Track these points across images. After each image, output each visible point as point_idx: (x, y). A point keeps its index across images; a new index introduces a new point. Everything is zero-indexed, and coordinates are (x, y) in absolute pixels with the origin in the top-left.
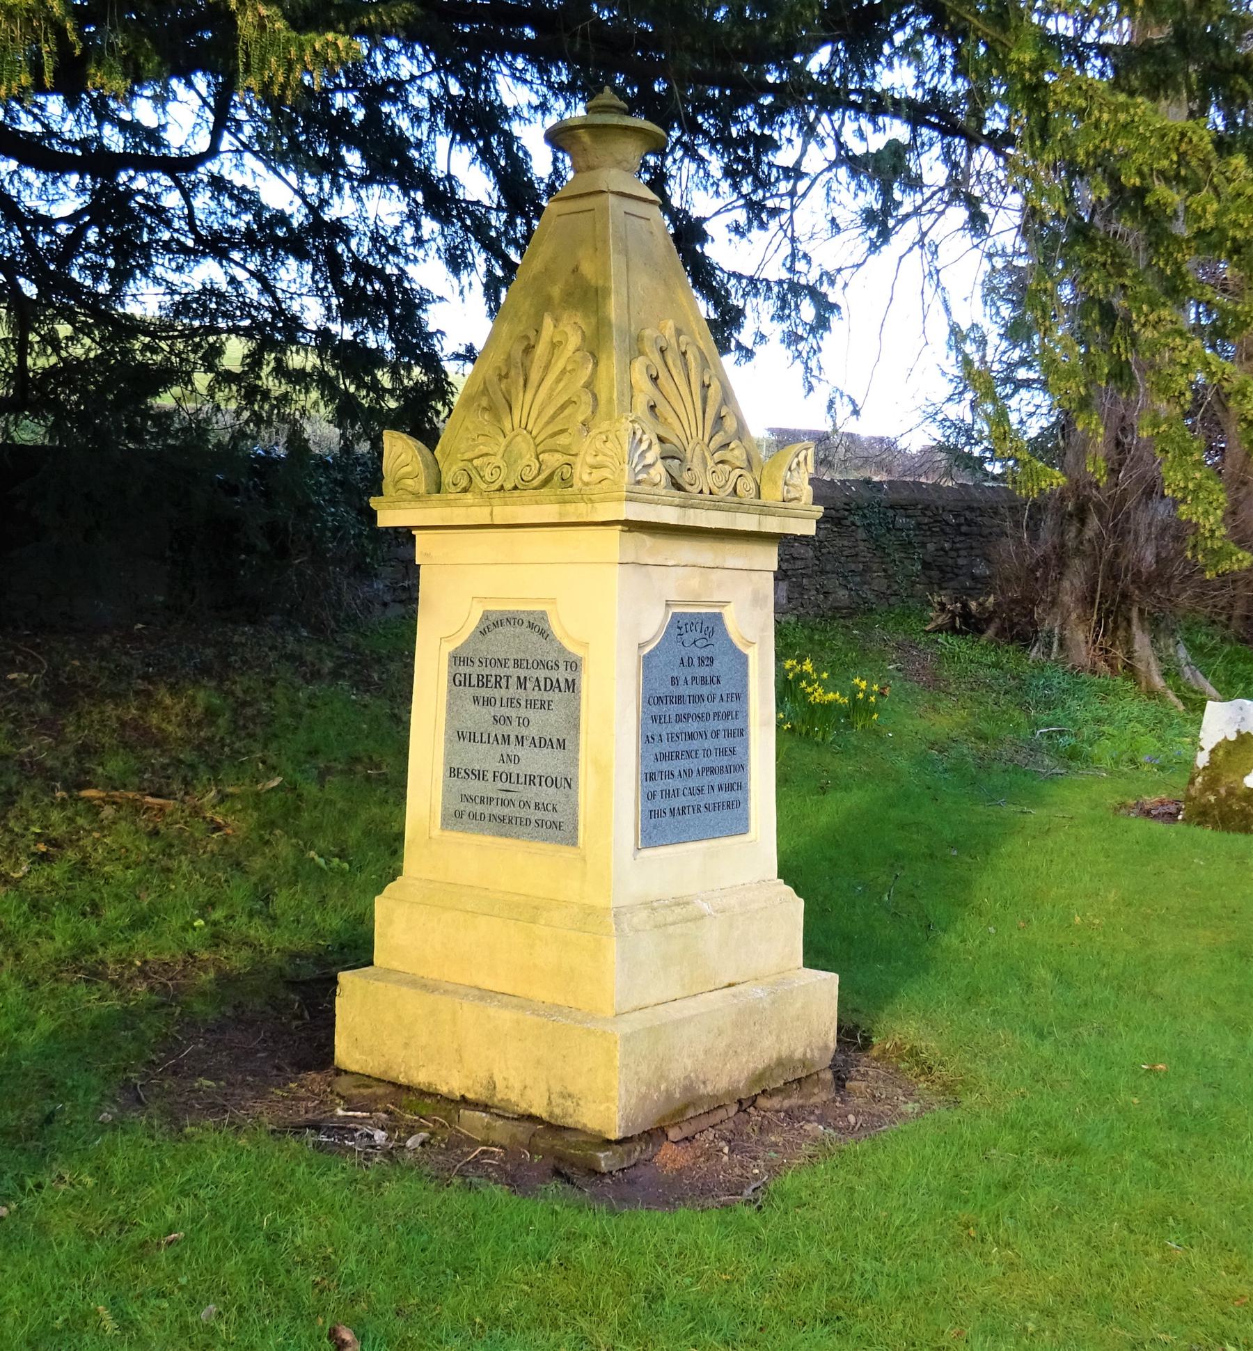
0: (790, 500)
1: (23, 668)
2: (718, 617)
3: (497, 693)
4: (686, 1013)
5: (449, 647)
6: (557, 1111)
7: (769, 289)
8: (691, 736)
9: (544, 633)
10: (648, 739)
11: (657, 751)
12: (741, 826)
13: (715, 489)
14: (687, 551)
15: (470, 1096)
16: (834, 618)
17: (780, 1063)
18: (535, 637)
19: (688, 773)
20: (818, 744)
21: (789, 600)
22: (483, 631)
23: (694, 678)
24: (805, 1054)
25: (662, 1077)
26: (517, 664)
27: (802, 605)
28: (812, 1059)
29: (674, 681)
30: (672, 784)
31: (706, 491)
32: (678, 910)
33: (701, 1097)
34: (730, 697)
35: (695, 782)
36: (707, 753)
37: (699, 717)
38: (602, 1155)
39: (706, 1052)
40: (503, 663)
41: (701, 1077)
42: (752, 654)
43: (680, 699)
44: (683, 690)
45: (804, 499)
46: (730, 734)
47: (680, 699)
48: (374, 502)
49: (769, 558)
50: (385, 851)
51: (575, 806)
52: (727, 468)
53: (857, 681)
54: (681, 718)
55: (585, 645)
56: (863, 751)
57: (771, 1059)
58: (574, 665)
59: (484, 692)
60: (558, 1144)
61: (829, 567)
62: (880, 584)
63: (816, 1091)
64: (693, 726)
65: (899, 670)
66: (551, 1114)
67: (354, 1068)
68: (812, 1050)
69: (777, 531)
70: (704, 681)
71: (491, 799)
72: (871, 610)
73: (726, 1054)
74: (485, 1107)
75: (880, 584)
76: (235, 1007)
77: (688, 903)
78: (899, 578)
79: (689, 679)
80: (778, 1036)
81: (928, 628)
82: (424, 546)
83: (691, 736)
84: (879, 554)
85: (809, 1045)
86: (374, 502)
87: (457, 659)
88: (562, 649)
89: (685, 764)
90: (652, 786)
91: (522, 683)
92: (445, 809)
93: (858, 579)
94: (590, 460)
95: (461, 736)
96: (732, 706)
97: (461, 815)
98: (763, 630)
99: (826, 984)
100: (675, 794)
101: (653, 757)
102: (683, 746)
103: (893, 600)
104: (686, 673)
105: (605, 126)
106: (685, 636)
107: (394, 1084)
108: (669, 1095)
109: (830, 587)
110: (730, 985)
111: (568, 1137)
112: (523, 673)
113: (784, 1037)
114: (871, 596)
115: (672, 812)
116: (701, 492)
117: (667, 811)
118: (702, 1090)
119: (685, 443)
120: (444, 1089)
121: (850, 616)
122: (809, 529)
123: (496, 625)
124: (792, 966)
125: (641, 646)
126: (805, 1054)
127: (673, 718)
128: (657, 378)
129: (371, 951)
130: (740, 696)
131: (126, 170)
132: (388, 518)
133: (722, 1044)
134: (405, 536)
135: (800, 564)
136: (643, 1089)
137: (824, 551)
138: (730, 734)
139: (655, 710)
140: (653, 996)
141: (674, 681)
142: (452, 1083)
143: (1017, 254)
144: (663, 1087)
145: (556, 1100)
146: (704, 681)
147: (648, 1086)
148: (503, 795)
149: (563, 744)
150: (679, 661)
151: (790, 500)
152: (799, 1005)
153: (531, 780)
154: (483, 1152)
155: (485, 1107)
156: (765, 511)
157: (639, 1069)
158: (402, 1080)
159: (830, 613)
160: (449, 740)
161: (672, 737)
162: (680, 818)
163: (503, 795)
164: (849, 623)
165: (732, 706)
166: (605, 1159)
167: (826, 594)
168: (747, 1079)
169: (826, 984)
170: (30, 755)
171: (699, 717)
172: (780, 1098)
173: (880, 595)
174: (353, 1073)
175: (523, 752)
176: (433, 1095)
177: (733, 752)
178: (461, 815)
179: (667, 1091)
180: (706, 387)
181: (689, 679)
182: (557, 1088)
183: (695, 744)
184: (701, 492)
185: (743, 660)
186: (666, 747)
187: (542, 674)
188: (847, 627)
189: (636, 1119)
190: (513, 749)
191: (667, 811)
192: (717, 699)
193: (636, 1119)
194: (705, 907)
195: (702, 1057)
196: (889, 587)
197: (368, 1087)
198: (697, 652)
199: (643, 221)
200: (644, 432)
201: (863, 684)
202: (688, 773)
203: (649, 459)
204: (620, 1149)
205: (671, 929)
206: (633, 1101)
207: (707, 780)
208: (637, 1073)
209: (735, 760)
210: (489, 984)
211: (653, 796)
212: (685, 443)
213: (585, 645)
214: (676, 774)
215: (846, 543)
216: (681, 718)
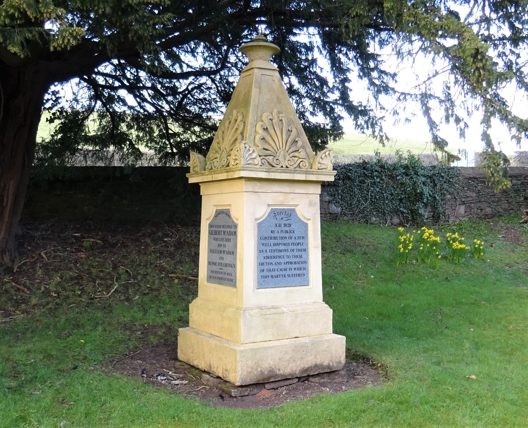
0: (322, 169)
1: (171, 237)
2: (294, 210)
3: (219, 237)
4: (271, 345)
5: (208, 222)
6: (225, 375)
7: (417, 96)
8: (281, 251)
9: (229, 216)
10: (260, 251)
11: (265, 256)
12: (306, 283)
13: (288, 166)
14: (276, 187)
15: (206, 370)
16: (485, 219)
17: (316, 366)
18: (227, 217)
19: (280, 264)
20: (456, 264)
21: (465, 212)
22: (216, 216)
23: (282, 231)
24: (329, 364)
25: (258, 366)
26: (223, 226)
27: (471, 214)
28: (333, 366)
29: (272, 232)
30: (272, 267)
31: (284, 166)
32: (273, 310)
33: (276, 375)
34: (299, 238)
35: (283, 266)
36: (288, 257)
37: (285, 244)
38: (232, 390)
39: (279, 359)
40: (220, 226)
41: (278, 368)
42: (310, 223)
43: (275, 238)
44: (276, 235)
45: (328, 169)
46: (300, 250)
47: (275, 238)
48: (187, 175)
49: (318, 190)
50: (190, 288)
51: (236, 274)
52: (296, 159)
53: (476, 240)
54: (275, 245)
55: (238, 219)
56: (474, 266)
57: (312, 364)
58: (236, 226)
59: (216, 236)
60: (223, 386)
61: (482, 200)
62: (506, 206)
63: (336, 377)
64: (282, 247)
65: (503, 237)
66: (223, 376)
67: (182, 360)
68: (333, 363)
69: (273, 178)
70: (287, 232)
71: (217, 272)
72: (501, 216)
73: (289, 361)
74: (209, 373)
75: (506, 206)
76: (165, 340)
77: (278, 308)
78: (514, 203)
79: (280, 231)
80: (315, 356)
81: (521, 222)
82: (203, 191)
83: (281, 251)
84: (504, 194)
85: (332, 360)
86: (187, 175)
87: (210, 226)
88: (233, 221)
89: (278, 260)
90: (262, 267)
91: (224, 232)
92: (208, 275)
93: (495, 204)
94: (234, 157)
95: (211, 251)
96: (301, 241)
97: (210, 278)
98: (314, 214)
99: (342, 339)
100: (274, 270)
101: (263, 258)
102: (276, 254)
103: (511, 212)
104: (277, 229)
105: (253, 46)
106: (277, 216)
107: (190, 365)
108: (262, 373)
109: (483, 207)
110: (296, 337)
111: (228, 384)
112: (224, 229)
113: (318, 357)
114: (500, 210)
115: (272, 277)
116: (282, 167)
117: (270, 276)
118: (278, 372)
119: (277, 150)
120: (200, 367)
121: (492, 217)
122: (332, 179)
123: (226, 214)
124: (327, 332)
125: (256, 220)
126: (329, 364)
127: (272, 245)
128: (267, 128)
129: (188, 323)
130: (305, 237)
131: (166, 79)
132: (192, 180)
133: (287, 357)
134: (197, 187)
135: (470, 199)
136: (250, 370)
137: (481, 194)
138: (300, 250)
139: (264, 241)
140: (260, 338)
141: (272, 232)
142: (202, 366)
143: (128, 70)
144: (259, 370)
145: (225, 372)
146: (287, 232)
147: (252, 368)
148: (220, 270)
149: (233, 253)
150: (275, 225)
151: (322, 169)
152: (325, 346)
153: (226, 265)
154: (204, 388)
155: (209, 373)
156: (307, 173)
157: (247, 362)
158: (192, 364)
159: (483, 217)
160: (208, 253)
161: (271, 251)
162: (276, 279)
163: (220, 270)
164: (490, 220)
165: (301, 241)
166: (234, 392)
167: (481, 210)
168: (300, 370)
169: (342, 339)
170: (160, 263)
171: (285, 244)
172: (318, 378)
173: (505, 210)
174: (180, 361)
175: (224, 256)
176: (198, 369)
177: (301, 257)
178: (210, 278)
179: (261, 371)
180: (290, 131)
181: (280, 231)
182: (224, 368)
183: (282, 254)
184: (282, 167)
185: (306, 225)
186: (269, 254)
187: (229, 230)
188: (489, 222)
189: (247, 379)
190: (222, 255)
191: (270, 276)
192: (293, 238)
193: (247, 379)
194: (285, 310)
195: (277, 361)
196: (509, 207)
197: (183, 366)
198: (283, 222)
199: (270, 77)
200: (250, 147)
201: (479, 242)
202: (280, 264)
203: (254, 155)
204: (240, 389)
205: (267, 316)
206: (245, 373)
207: (288, 266)
208: (247, 364)
209: (302, 260)
210: (214, 333)
211: (263, 271)
212: (277, 150)
213: (238, 219)
214: (274, 263)
215: (490, 191)
216: (275, 245)
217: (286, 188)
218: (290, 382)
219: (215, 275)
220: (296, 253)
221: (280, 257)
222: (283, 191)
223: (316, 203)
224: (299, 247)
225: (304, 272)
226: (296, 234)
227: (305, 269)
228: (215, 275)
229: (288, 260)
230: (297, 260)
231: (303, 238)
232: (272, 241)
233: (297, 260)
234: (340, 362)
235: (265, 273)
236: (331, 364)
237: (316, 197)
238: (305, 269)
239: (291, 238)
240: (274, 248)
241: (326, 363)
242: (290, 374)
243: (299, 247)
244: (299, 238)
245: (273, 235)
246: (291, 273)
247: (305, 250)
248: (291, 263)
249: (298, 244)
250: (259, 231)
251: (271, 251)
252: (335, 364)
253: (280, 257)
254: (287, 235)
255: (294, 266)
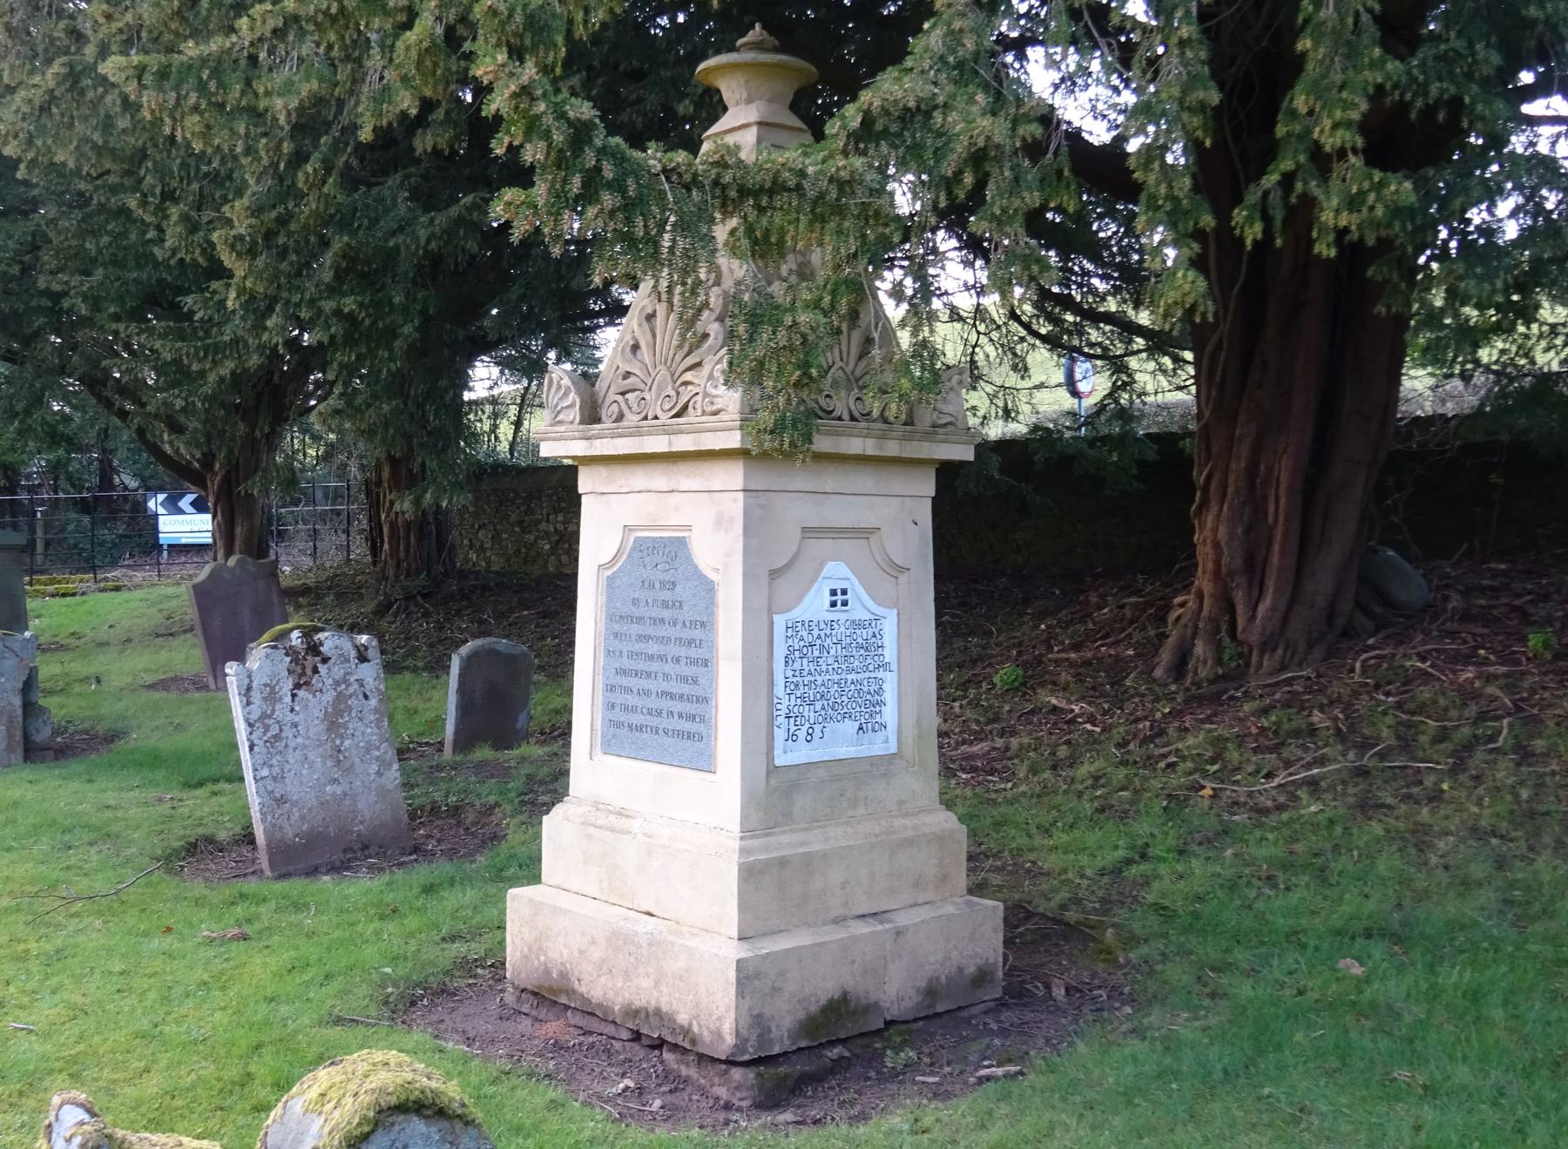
8: (651, 657)
29: (635, 602)
33: (574, 991)
34: (693, 624)
35: (654, 703)
43: (640, 620)
44: (642, 611)
47: (640, 620)
64: (653, 648)
70: (665, 605)
85: (697, 1017)
89: (644, 683)
96: (697, 634)
102: (642, 666)
130: (706, 624)
146: (665, 605)
165: (697, 634)
177: (695, 682)
183: (655, 666)
186: (626, 663)
195: (576, 954)
207: (666, 704)
217: (658, 478)
218: (595, 1025)
219: (625, 681)
220: (688, 671)
221: (649, 675)
222: (653, 486)
223: (732, 519)
224: (693, 653)
225: (702, 728)
226: (687, 614)
227: (703, 720)
228: (625, 681)
229: (666, 686)
230: (686, 689)
231: (703, 625)
232: (635, 629)
233: (686, 689)
234: (719, 1035)
235: (618, 715)
236: (695, 1029)
237: (735, 500)
238: (703, 720)
239: (675, 624)
240: (638, 647)
241: (682, 1018)
242: (600, 1005)
243: (693, 653)
244: (693, 624)
245: (637, 612)
246: (664, 723)
247: (706, 663)
248: (671, 696)
249: (690, 642)
250: (610, 599)
251: (633, 655)
252: (706, 1033)
253: (649, 675)
254: (666, 614)
255: (678, 707)
